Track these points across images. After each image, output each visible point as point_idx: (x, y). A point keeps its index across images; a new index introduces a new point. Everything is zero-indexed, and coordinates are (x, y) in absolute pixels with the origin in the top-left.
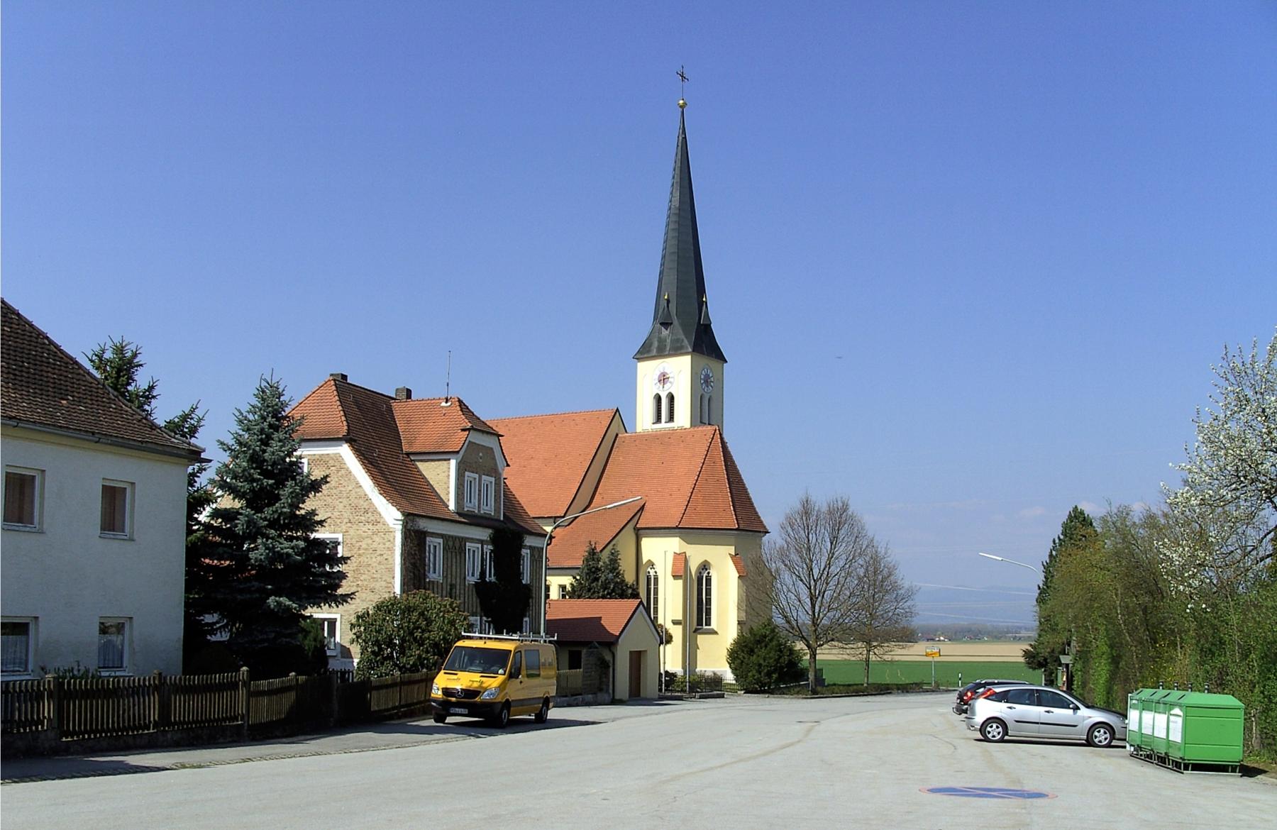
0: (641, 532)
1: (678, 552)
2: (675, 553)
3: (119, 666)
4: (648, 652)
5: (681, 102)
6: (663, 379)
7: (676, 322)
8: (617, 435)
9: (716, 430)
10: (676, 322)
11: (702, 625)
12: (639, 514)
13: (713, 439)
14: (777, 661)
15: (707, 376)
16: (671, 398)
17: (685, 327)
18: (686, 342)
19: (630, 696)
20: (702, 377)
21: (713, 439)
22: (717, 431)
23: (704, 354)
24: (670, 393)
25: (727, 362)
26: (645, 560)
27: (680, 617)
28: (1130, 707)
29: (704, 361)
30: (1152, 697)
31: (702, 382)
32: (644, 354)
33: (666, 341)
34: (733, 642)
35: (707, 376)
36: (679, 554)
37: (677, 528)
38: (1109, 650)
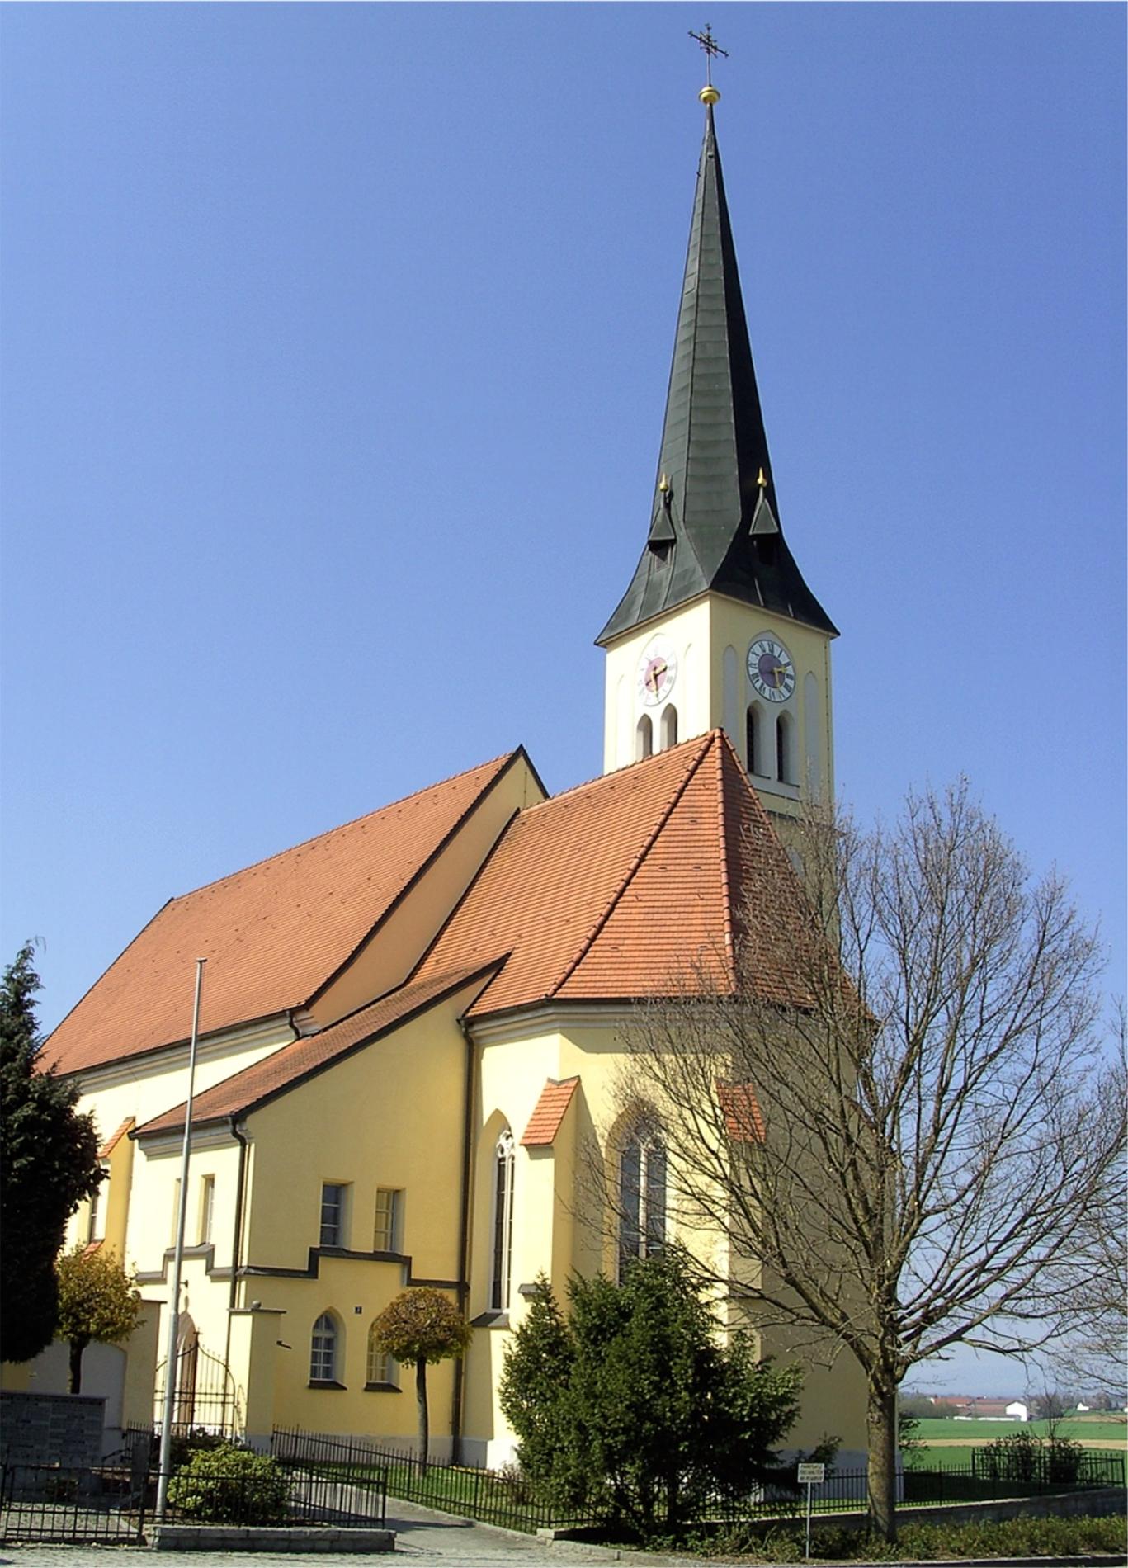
0: (480, 1029)
1: (558, 1079)
5: (705, 91)
6: (656, 676)
8: (518, 811)
13: (700, 761)
14: (641, 1409)
18: (699, 572)
20: (753, 659)
21: (700, 761)
22: (717, 743)
23: (752, 599)
24: (670, 705)
25: (839, 634)
26: (487, 1113)
31: (753, 671)
32: (617, 627)
33: (661, 584)
34: (13, 1363)
36: (562, 1082)
37: (549, 1002)
38: (881, 1413)
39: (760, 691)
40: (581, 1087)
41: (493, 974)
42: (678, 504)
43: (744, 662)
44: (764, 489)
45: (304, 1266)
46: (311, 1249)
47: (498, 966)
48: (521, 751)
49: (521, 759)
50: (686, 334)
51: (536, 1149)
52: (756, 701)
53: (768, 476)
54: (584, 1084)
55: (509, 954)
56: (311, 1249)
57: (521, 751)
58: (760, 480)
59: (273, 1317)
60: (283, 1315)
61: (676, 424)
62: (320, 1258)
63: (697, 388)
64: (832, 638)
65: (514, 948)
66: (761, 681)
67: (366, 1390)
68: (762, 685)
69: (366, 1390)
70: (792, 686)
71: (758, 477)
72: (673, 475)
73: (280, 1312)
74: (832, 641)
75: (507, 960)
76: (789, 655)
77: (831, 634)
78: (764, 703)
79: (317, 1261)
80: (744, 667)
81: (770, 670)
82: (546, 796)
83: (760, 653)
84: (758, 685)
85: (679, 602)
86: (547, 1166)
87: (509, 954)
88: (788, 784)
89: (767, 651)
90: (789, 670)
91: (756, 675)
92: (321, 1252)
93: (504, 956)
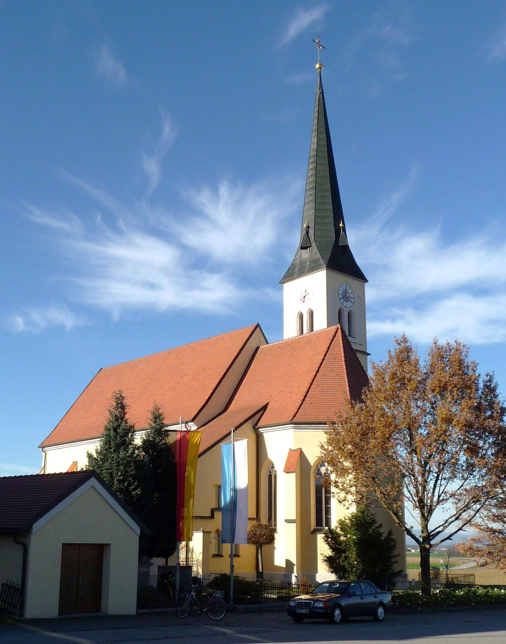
1: (293, 449)
2: (290, 449)
3: (474, 576)
4: (112, 545)
7: (314, 245)
9: (338, 329)
10: (314, 245)
11: (322, 526)
12: (262, 412)
15: (345, 292)
16: (311, 314)
17: (320, 249)
18: (322, 262)
19: (141, 603)
20: (340, 292)
22: (339, 330)
27: (293, 517)
28: (283, 340)
29: (341, 278)
30: (292, 421)
31: (340, 296)
35: (345, 292)
39: (342, 304)
40: (302, 451)
41: (263, 410)
42: (311, 232)
43: (337, 293)
44: (342, 227)
45: (209, 515)
46: (212, 509)
47: (265, 408)
48: (258, 325)
49: (258, 328)
50: (312, 166)
51: (287, 471)
52: (341, 307)
53: (343, 223)
54: (302, 450)
55: (268, 403)
56: (212, 509)
57: (258, 325)
58: (341, 225)
59: (208, 534)
60: (211, 533)
61: (309, 201)
62: (215, 512)
63: (317, 188)
64: (366, 283)
65: (270, 401)
66: (343, 300)
67: (213, 557)
68: (343, 301)
69: (213, 557)
70: (353, 301)
71: (340, 224)
72: (310, 220)
73: (210, 532)
74: (366, 284)
75: (267, 405)
76: (352, 290)
77: (365, 281)
78: (343, 307)
79: (214, 513)
80: (337, 295)
81: (345, 297)
82: (268, 343)
83: (342, 290)
84: (342, 302)
85: (313, 268)
86: (293, 476)
87: (268, 403)
88: (352, 337)
89: (345, 289)
90: (352, 296)
91: (341, 298)
92: (215, 510)
93: (266, 405)
